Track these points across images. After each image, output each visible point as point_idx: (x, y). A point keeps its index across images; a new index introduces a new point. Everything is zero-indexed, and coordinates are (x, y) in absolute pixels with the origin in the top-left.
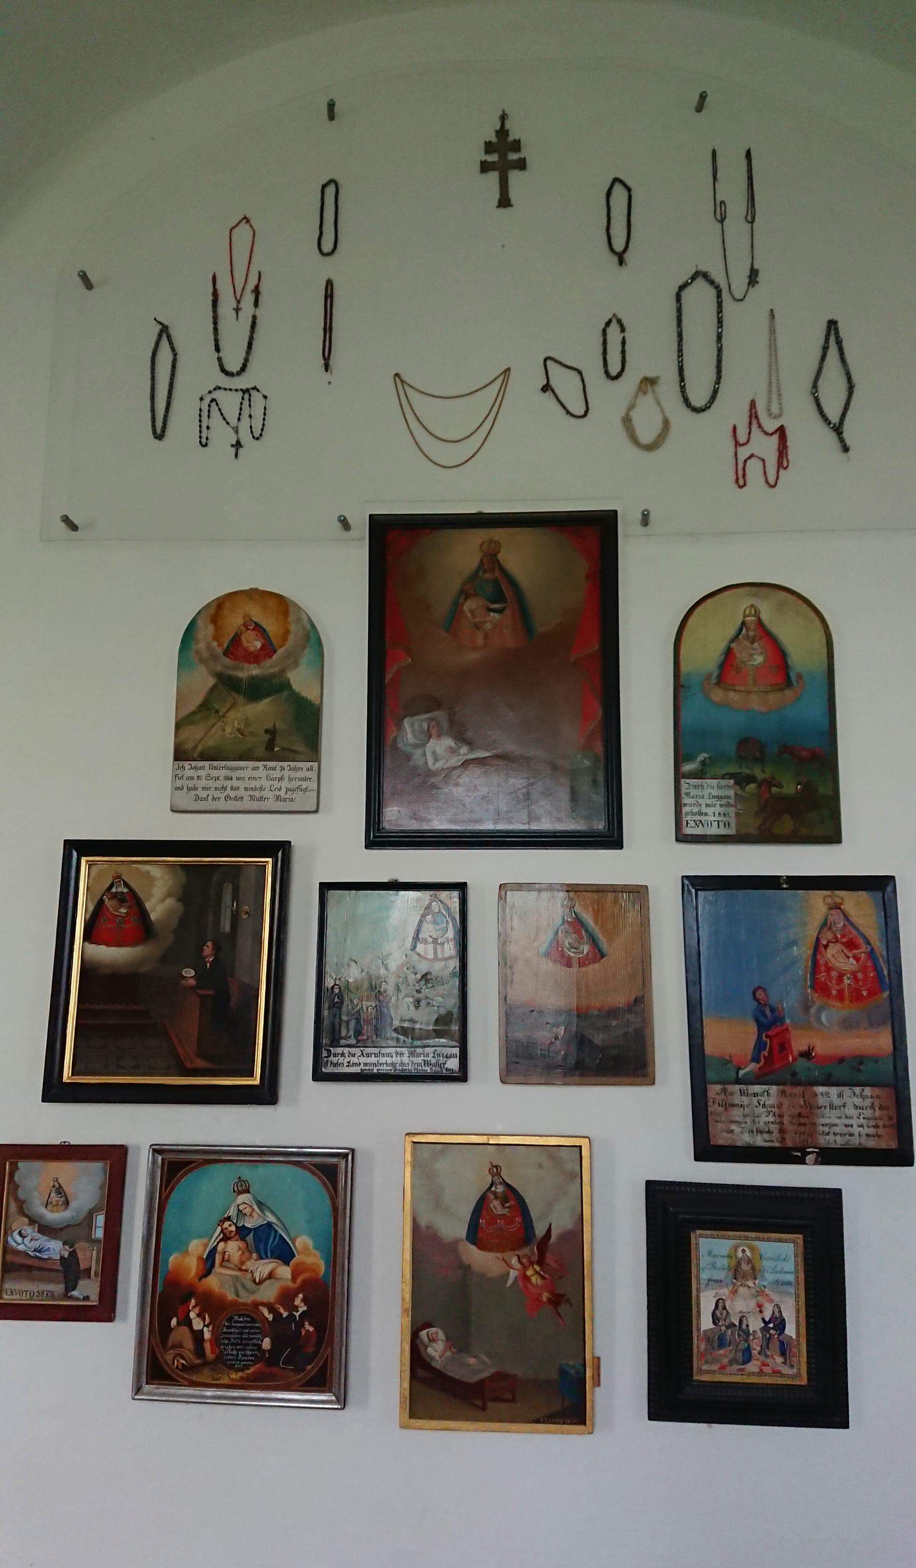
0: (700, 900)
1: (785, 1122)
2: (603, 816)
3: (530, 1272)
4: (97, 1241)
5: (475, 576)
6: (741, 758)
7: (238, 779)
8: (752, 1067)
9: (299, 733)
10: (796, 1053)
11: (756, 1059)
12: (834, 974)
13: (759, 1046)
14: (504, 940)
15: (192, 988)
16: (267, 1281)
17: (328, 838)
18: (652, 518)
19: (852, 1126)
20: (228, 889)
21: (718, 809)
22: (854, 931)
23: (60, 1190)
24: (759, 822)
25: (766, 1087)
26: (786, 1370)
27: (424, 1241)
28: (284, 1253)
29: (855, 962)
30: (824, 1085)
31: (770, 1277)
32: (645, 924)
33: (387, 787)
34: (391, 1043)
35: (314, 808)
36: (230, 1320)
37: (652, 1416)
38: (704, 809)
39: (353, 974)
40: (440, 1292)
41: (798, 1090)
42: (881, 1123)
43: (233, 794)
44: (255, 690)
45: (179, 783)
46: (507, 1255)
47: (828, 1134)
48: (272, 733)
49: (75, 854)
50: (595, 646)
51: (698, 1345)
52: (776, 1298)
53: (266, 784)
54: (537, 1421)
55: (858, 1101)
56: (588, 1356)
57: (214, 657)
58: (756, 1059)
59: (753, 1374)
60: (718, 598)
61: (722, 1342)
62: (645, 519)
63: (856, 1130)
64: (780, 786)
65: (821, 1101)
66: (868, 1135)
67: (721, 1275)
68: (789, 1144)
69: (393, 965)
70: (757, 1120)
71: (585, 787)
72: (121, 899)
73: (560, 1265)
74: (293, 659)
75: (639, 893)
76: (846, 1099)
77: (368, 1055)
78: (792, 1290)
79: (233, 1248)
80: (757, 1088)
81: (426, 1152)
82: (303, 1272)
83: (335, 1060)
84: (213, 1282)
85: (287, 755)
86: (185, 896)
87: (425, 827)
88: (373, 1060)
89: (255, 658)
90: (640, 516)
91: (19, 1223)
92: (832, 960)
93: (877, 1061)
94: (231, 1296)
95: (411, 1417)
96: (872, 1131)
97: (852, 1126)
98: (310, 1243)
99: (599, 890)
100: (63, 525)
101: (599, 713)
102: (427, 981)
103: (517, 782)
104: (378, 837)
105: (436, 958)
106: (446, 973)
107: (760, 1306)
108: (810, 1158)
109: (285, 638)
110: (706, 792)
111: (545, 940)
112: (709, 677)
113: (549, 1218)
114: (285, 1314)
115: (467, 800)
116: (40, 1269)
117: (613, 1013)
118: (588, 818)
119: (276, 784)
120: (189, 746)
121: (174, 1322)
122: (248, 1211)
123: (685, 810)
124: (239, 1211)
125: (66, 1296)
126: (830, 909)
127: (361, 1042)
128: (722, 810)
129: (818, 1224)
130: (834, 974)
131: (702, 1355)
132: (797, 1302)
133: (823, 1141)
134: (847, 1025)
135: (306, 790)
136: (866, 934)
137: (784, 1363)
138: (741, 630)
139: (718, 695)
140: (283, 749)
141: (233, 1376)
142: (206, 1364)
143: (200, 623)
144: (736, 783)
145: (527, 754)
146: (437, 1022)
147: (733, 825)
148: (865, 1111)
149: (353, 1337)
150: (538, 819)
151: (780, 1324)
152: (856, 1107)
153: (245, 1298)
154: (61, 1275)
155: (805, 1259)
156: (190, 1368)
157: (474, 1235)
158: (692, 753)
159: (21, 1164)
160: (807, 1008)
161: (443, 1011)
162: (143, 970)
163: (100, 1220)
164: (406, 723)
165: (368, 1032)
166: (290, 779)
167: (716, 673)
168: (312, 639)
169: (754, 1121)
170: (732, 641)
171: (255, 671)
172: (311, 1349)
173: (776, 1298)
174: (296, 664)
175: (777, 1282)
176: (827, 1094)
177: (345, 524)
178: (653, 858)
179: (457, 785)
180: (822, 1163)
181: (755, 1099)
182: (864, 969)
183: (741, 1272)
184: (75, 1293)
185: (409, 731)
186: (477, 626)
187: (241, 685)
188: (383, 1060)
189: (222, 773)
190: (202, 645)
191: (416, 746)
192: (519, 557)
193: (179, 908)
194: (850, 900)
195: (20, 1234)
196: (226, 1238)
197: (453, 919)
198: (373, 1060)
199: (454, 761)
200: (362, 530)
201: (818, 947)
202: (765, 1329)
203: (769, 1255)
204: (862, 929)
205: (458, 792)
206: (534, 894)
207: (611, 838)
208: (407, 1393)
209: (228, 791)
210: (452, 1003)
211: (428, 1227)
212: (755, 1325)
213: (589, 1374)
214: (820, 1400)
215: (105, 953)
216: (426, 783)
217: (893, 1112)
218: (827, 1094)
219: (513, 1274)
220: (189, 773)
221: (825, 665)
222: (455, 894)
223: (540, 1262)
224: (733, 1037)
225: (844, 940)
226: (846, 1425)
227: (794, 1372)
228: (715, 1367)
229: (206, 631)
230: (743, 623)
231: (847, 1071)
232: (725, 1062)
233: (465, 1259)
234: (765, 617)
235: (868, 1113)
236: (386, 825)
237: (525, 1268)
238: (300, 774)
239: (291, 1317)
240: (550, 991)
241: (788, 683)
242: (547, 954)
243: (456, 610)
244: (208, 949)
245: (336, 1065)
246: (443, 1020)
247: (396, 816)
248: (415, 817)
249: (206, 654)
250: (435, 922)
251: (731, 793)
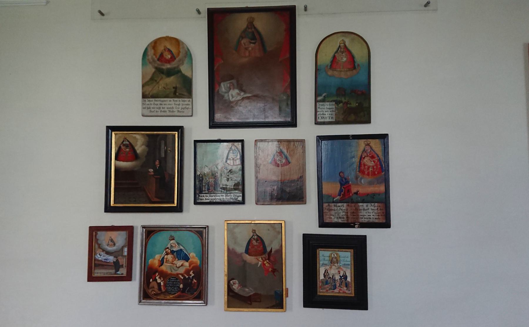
0: (323, 144)
2: (290, 116)
3: (265, 262)
4: (125, 256)
5: (245, 31)
6: (338, 95)
7: (164, 104)
8: (338, 197)
9: (185, 89)
11: (339, 195)
13: (341, 191)
14: (256, 159)
15: (153, 175)
16: (181, 267)
17: (197, 126)
18: (308, 8)
20: (163, 143)
21: (329, 113)
23: (112, 240)
24: (343, 117)
26: (347, 292)
27: (231, 253)
28: (186, 258)
30: (361, 203)
31: (342, 263)
32: (304, 152)
33: (216, 107)
34: (219, 192)
35: (191, 115)
36: (169, 279)
37: (305, 306)
38: (324, 113)
39: (206, 170)
40: (236, 269)
41: (353, 205)
42: (380, 214)
43: (163, 110)
44: (169, 73)
45: (144, 106)
46: (258, 257)
48: (175, 88)
49: (110, 131)
50: (288, 56)
51: (319, 284)
52: (344, 269)
53: (174, 106)
54: (268, 308)
55: (373, 208)
56: (284, 288)
57: (154, 61)
58: (339, 195)
59: (337, 293)
60: (331, 37)
61: (327, 283)
62: (306, 9)
63: (372, 217)
64: (350, 104)
65: (361, 208)
67: (326, 262)
68: (350, 222)
69: (220, 167)
71: (284, 106)
72: (127, 146)
73: (275, 261)
74: (182, 62)
75: (303, 141)
76: (369, 207)
77: (212, 196)
78: (350, 267)
79: (170, 257)
80: (340, 204)
81: (231, 226)
82: (193, 264)
83: (201, 198)
84: (163, 268)
85: (181, 96)
86: (148, 145)
87: (229, 121)
88: (214, 198)
89: (168, 61)
90: (303, 8)
91: (99, 251)
94: (169, 272)
95: (228, 307)
96: (377, 217)
98: (195, 255)
99: (289, 141)
100: (99, 14)
101: (289, 80)
102: (231, 172)
103: (261, 105)
104: (213, 125)
105: (234, 165)
106: (237, 170)
107: (339, 272)
108: (356, 226)
109: (178, 54)
110: (325, 107)
111: (270, 159)
112: (327, 66)
113: (272, 246)
114: (187, 277)
115: (244, 111)
116: (106, 265)
117: (293, 181)
118: (285, 117)
119: (177, 106)
120: (147, 93)
121: (151, 280)
122: (174, 245)
123: (318, 113)
124: (171, 246)
125: (115, 273)
127: (209, 192)
128: (330, 113)
129: (359, 247)
130: (366, 167)
131: (320, 287)
132: (351, 270)
133: (361, 220)
134: (370, 183)
135: (188, 108)
137: (347, 289)
138: (338, 49)
139: (330, 73)
140: (180, 94)
141: (171, 296)
142: (162, 293)
143: (149, 49)
144: (336, 103)
145: (265, 95)
146: (234, 186)
147: (334, 118)
149: (209, 275)
150: (268, 117)
151: (346, 277)
152: (372, 209)
153: (174, 272)
154: (114, 267)
155: (354, 257)
156: (156, 295)
157: (247, 251)
158: (321, 93)
159: (98, 233)
160: (357, 178)
161: (236, 182)
162: (136, 169)
163: (126, 250)
164: (222, 84)
165: (212, 188)
166: (182, 105)
167: (330, 64)
168: (188, 55)
170: (335, 53)
171: (168, 66)
172: (195, 288)
173: (344, 269)
174: (183, 64)
175: (345, 264)
176: (363, 206)
177: (199, 12)
178: (307, 130)
179: (240, 106)
180: (360, 228)
182: (376, 165)
183: (333, 261)
184: (118, 273)
185: (223, 87)
186: (246, 49)
187: (164, 71)
188: (217, 198)
189: (159, 103)
190: (150, 57)
191: (226, 93)
192: (261, 23)
193: (147, 149)
194: (373, 143)
195: (99, 255)
196: (167, 254)
197: (239, 152)
198: (214, 198)
199: (239, 98)
200: (205, 14)
201: (361, 158)
202: (341, 279)
203: (342, 256)
205: (241, 108)
206: (266, 143)
207: (293, 124)
208: (226, 300)
209: (161, 109)
210: (239, 179)
211: (233, 249)
212: (337, 277)
213: (284, 293)
214: (358, 300)
215: (123, 164)
216: (229, 106)
217: (384, 211)
218: (362, 206)
219: (260, 263)
220: (148, 103)
221: (368, 61)
222: (240, 144)
223: (269, 259)
224: (332, 188)
226: (366, 308)
227: (350, 292)
228: (324, 291)
229: (151, 52)
230: (340, 46)
231: (370, 198)
232: (329, 196)
233: (244, 259)
234: (347, 44)
235: (376, 211)
236: (216, 120)
237: (264, 261)
238: (186, 103)
239: (189, 278)
240: (271, 174)
241: (354, 68)
242: (271, 163)
243: (239, 42)
244: (157, 162)
245: (201, 199)
246: (236, 185)
247: (219, 117)
248: (226, 117)
249: (151, 60)
250: (233, 153)
251: (334, 107)
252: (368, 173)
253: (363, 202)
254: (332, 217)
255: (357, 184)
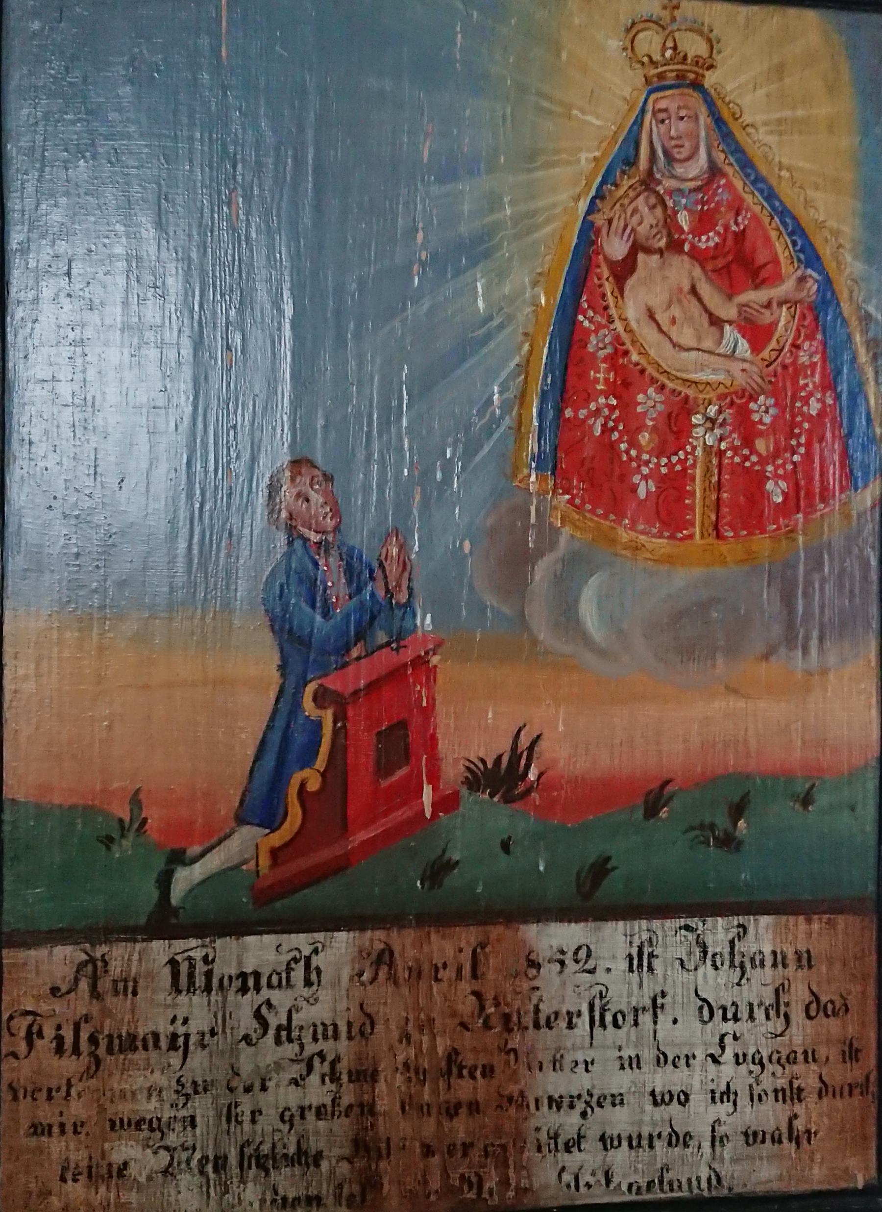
1: (381, 1106)
8: (244, 845)
10: (452, 772)
11: (261, 809)
12: (649, 403)
13: (284, 742)
19: (684, 1098)
22: (753, 201)
25: (302, 941)
29: (743, 346)
41: (449, 947)
42: (808, 1077)
47: (575, 1143)
55: (716, 984)
63: (700, 1116)
65: (559, 991)
66: (752, 1137)
70: (246, 1107)
76: (667, 975)
80: (261, 951)
92: (648, 334)
93: (806, 801)
96: (770, 1115)
97: (684, 1098)
126: (656, 85)
130: (649, 403)
134: (694, 637)
136: (807, 217)
148: (742, 1027)
169: (230, 1115)
176: (584, 955)
181: (248, 1003)
182: (783, 381)
201: (588, 276)
204: (788, 195)
218: (585, 959)
225: (708, 241)
235: (757, 1035)
252: (674, 485)
253: (592, 897)
254: (126, 1150)
255: (515, 645)
